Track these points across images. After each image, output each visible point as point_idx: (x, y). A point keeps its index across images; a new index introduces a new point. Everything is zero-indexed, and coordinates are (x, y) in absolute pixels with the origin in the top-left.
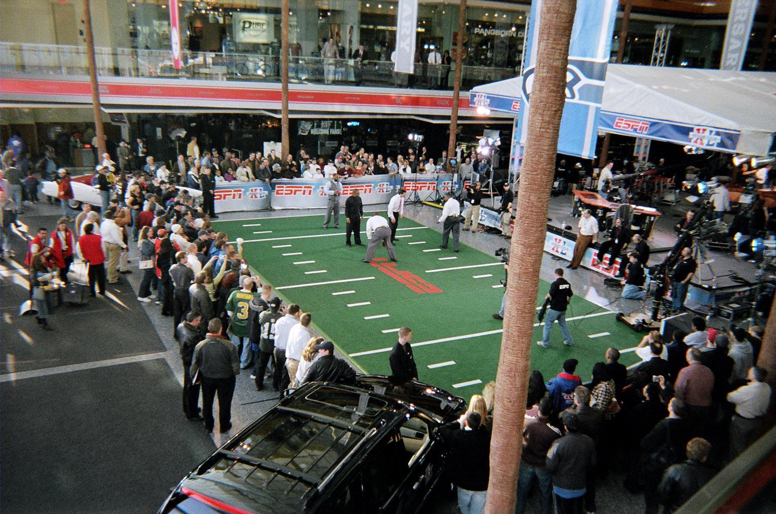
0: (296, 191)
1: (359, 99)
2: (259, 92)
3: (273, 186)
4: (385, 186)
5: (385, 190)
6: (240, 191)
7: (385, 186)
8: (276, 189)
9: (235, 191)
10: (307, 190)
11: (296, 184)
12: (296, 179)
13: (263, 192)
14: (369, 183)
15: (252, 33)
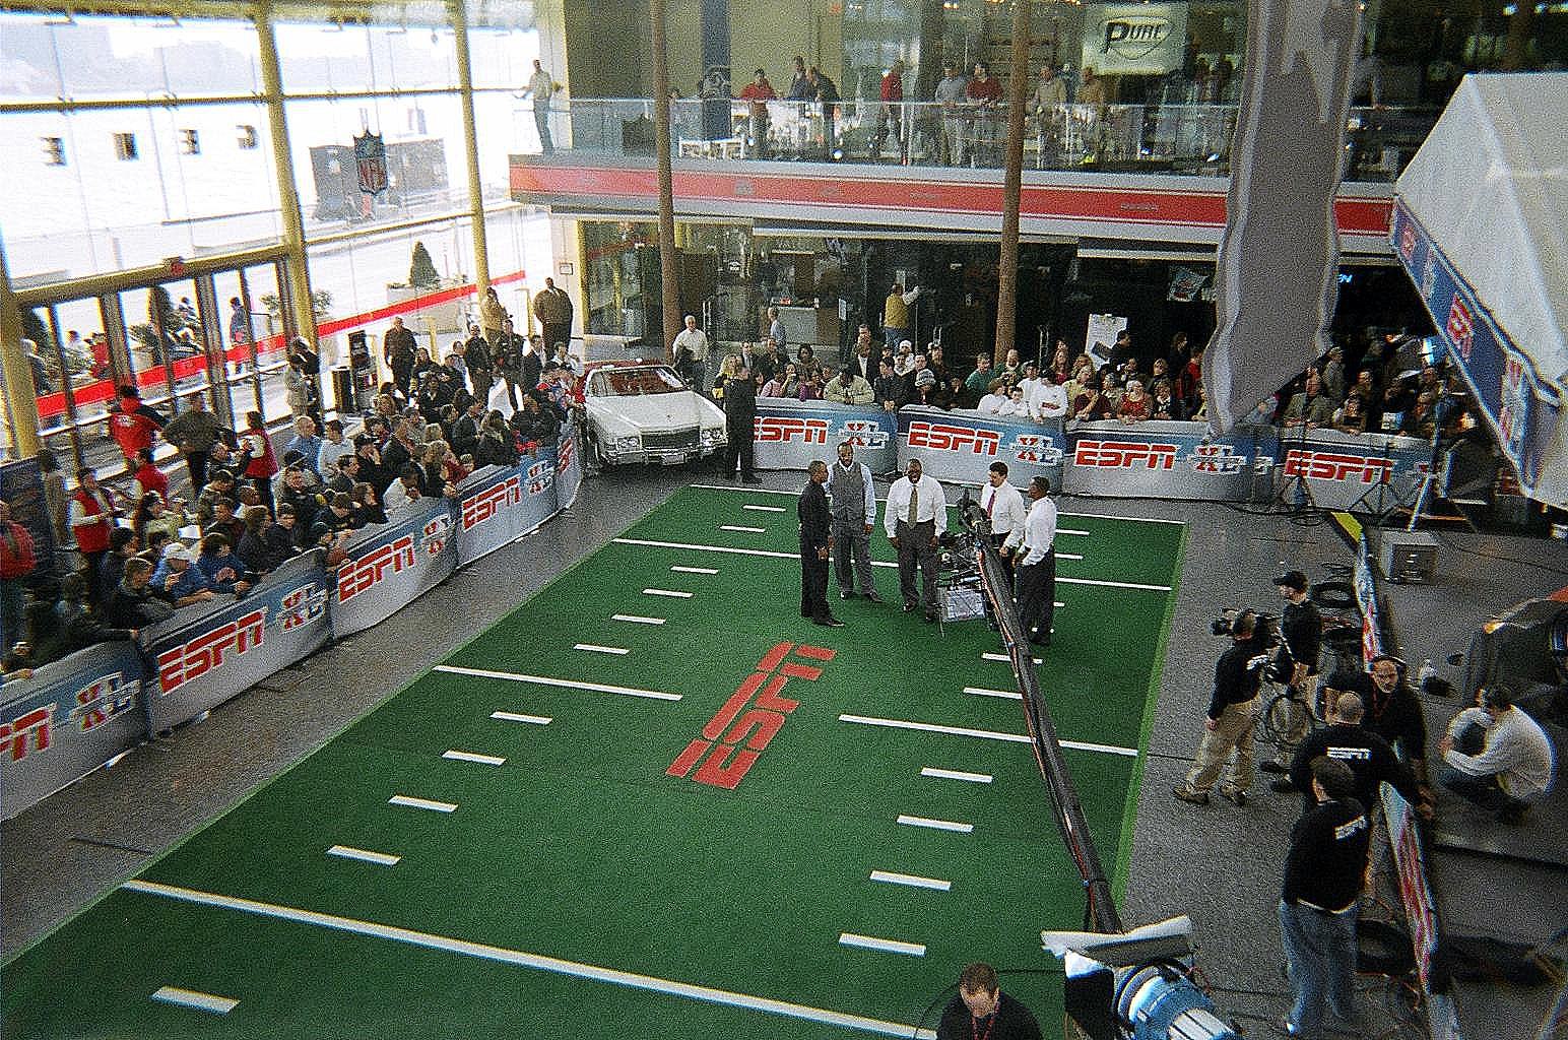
0: (1343, 469)
1: (1124, 206)
2: (1140, 199)
3: (903, 422)
4: (1220, 455)
5: (1219, 466)
6: (1172, 449)
7: (1220, 455)
8: (1078, 449)
9: (1155, 448)
10: (816, 430)
11: (962, 423)
12: (958, 412)
13: (1231, 456)
14: (993, 427)
15: (1134, 52)
